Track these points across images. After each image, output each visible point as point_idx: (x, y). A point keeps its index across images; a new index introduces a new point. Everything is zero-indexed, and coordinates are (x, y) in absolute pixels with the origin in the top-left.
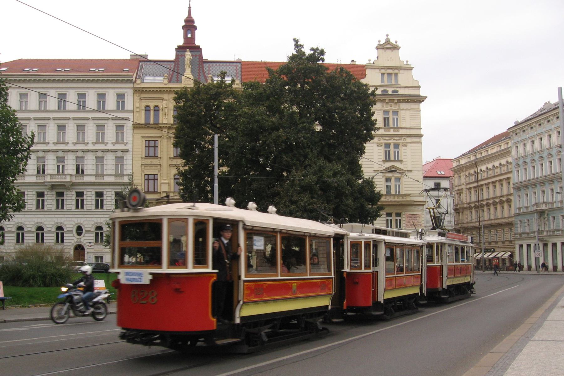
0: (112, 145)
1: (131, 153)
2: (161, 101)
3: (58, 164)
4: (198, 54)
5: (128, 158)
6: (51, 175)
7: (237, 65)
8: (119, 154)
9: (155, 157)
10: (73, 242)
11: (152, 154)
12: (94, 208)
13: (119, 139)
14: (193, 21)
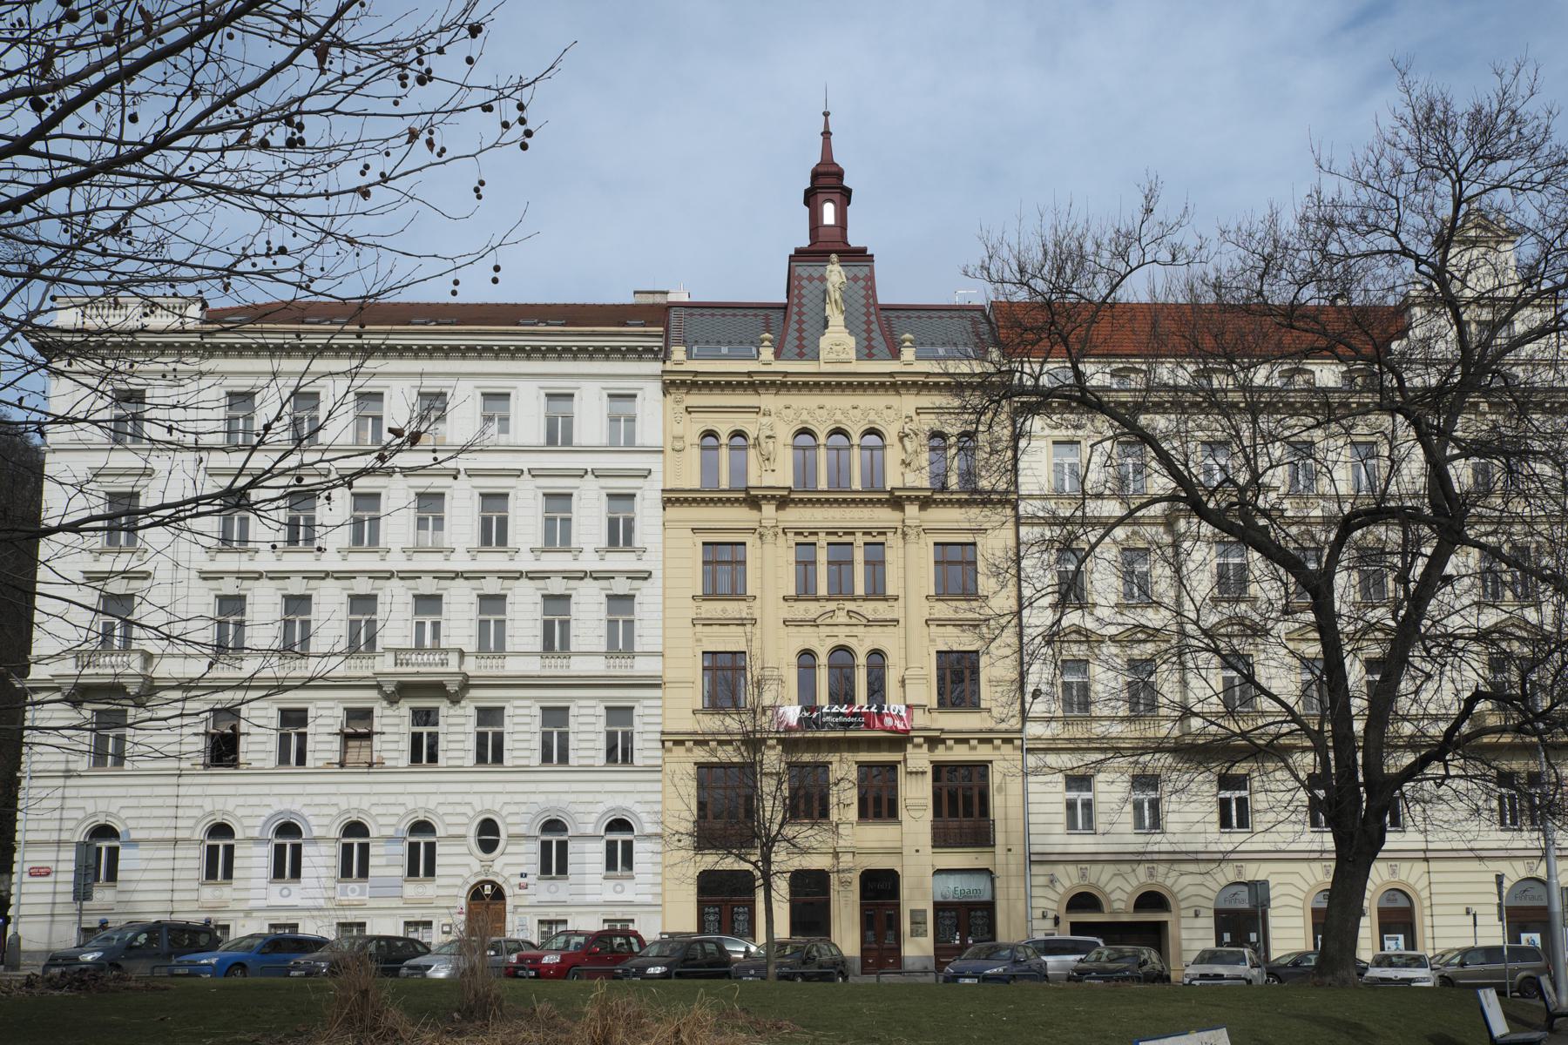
0: (338, 556)
1: (659, 583)
2: (754, 415)
3: (420, 618)
4: (861, 275)
5: (649, 600)
6: (396, 651)
8: (621, 586)
9: (737, 593)
10: (466, 872)
11: (724, 586)
12: (471, 759)
13: (620, 534)
14: (840, 174)
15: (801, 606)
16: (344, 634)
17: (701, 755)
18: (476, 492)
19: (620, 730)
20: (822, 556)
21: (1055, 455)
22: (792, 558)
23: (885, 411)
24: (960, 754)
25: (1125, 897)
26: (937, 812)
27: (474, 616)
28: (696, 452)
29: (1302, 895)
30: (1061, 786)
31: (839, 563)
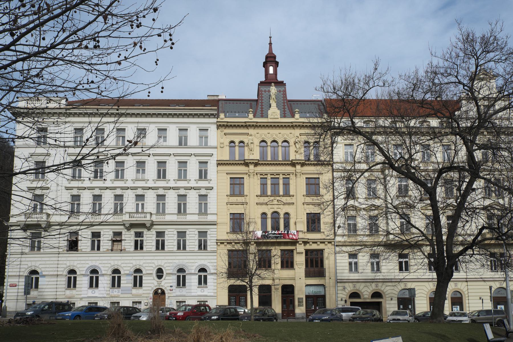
0: (111, 182)
2: (247, 136)
3: (137, 202)
4: (282, 90)
5: (212, 196)
7: (251, 103)
8: (203, 192)
9: (241, 194)
10: (152, 285)
11: (237, 192)
12: (154, 248)
13: (203, 175)
14: (275, 57)
15: (262, 198)
16: (112, 207)
17: (229, 247)
18: (156, 161)
19: (203, 239)
20: (269, 182)
21: (345, 149)
22: (259, 183)
23: (290, 135)
24: (314, 247)
25: (368, 294)
26: (307, 266)
27: (155, 202)
28: (228, 148)
29: (426, 293)
30: (347, 257)
31: (275, 184)
